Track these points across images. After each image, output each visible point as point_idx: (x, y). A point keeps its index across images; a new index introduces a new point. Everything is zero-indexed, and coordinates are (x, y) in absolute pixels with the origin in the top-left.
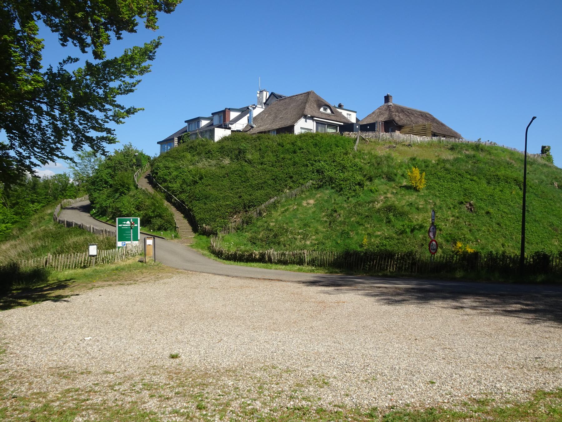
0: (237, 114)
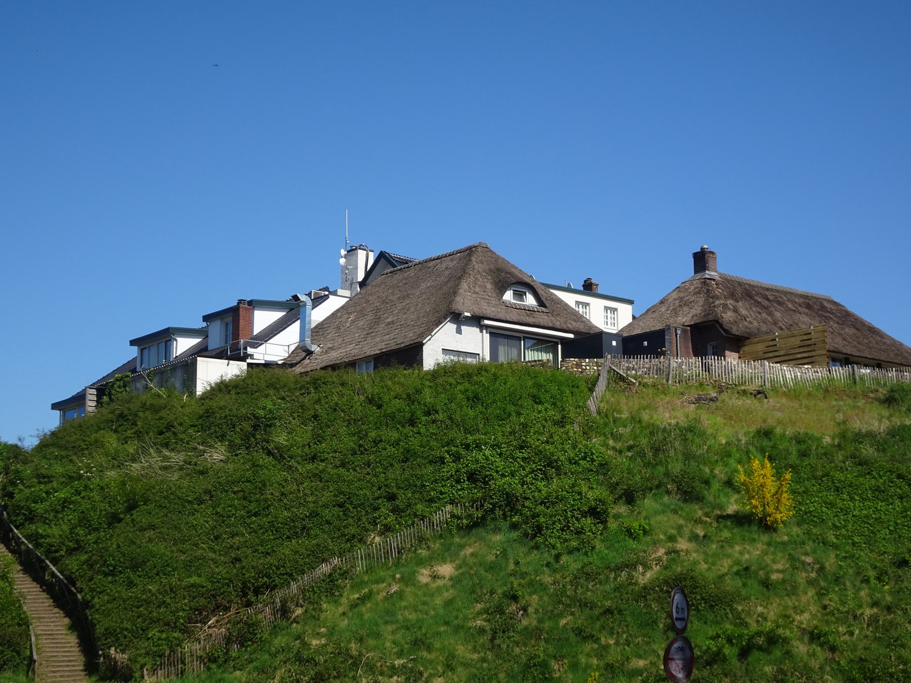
0: (275, 316)
